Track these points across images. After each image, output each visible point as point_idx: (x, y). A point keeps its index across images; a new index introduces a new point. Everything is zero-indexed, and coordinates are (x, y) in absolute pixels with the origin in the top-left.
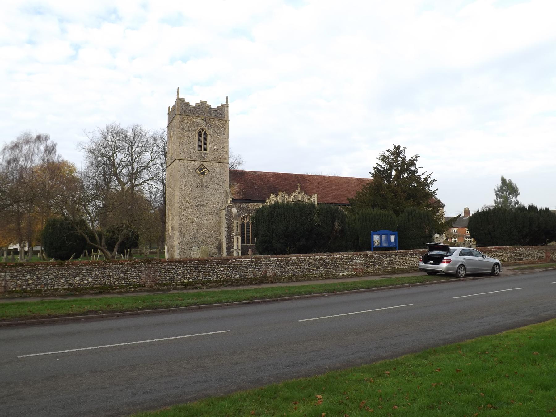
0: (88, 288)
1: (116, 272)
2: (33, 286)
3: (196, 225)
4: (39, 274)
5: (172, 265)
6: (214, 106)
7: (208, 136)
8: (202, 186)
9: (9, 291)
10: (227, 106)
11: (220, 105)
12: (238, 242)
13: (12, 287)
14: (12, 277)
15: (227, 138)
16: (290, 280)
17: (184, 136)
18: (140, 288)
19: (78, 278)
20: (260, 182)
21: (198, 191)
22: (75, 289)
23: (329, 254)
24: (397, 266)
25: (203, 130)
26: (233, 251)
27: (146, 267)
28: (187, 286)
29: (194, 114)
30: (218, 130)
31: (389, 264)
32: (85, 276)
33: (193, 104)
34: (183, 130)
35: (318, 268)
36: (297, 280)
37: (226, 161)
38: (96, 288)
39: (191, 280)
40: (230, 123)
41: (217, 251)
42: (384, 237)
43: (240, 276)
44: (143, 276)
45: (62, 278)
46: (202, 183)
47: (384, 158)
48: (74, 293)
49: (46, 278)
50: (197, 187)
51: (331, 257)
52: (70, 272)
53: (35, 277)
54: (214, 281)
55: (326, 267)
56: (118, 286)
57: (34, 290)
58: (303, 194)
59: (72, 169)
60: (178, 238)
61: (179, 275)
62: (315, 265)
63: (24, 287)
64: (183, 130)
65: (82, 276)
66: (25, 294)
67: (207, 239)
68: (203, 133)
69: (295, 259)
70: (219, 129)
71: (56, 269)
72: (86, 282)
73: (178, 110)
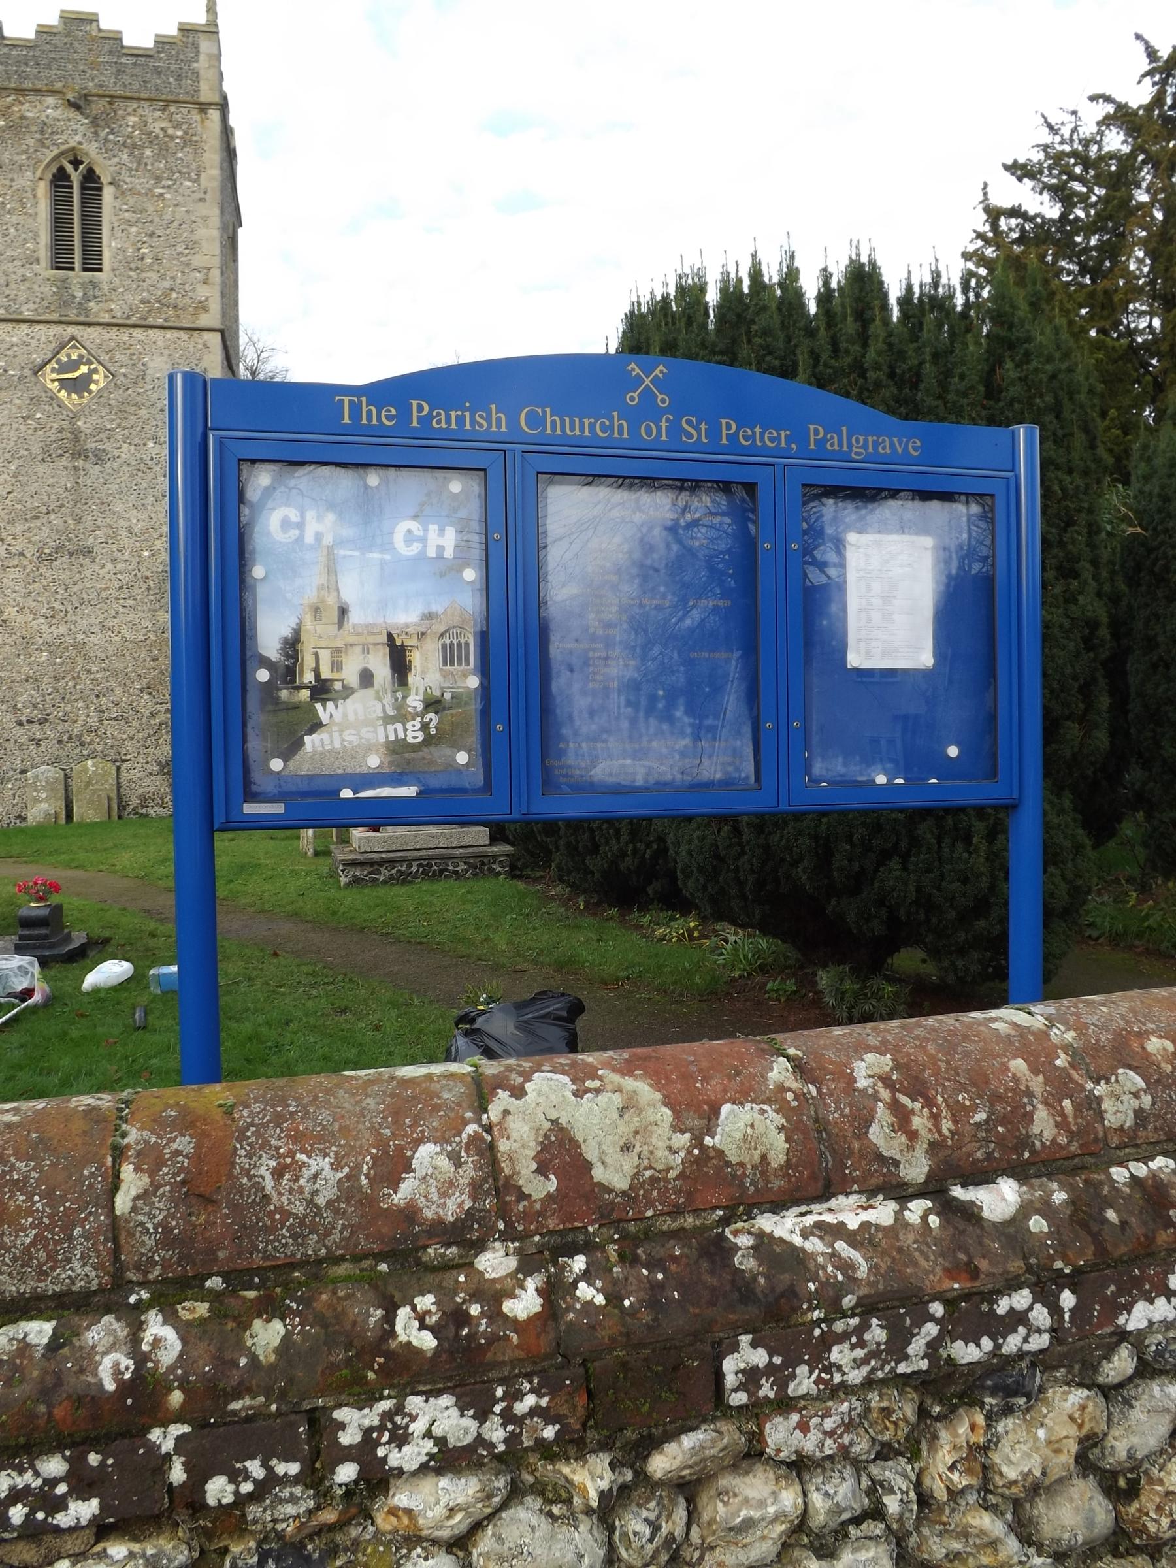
6: (139, 37)
7: (108, 193)
8: (76, 455)
10: (211, 30)
11: (53, 20)
21: (54, 478)
29: (22, 77)
30: (158, 156)
41: (165, 789)
46: (76, 435)
50: (47, 456)
67: (112, 728)
68: (76, 177)
70: (163, 151)
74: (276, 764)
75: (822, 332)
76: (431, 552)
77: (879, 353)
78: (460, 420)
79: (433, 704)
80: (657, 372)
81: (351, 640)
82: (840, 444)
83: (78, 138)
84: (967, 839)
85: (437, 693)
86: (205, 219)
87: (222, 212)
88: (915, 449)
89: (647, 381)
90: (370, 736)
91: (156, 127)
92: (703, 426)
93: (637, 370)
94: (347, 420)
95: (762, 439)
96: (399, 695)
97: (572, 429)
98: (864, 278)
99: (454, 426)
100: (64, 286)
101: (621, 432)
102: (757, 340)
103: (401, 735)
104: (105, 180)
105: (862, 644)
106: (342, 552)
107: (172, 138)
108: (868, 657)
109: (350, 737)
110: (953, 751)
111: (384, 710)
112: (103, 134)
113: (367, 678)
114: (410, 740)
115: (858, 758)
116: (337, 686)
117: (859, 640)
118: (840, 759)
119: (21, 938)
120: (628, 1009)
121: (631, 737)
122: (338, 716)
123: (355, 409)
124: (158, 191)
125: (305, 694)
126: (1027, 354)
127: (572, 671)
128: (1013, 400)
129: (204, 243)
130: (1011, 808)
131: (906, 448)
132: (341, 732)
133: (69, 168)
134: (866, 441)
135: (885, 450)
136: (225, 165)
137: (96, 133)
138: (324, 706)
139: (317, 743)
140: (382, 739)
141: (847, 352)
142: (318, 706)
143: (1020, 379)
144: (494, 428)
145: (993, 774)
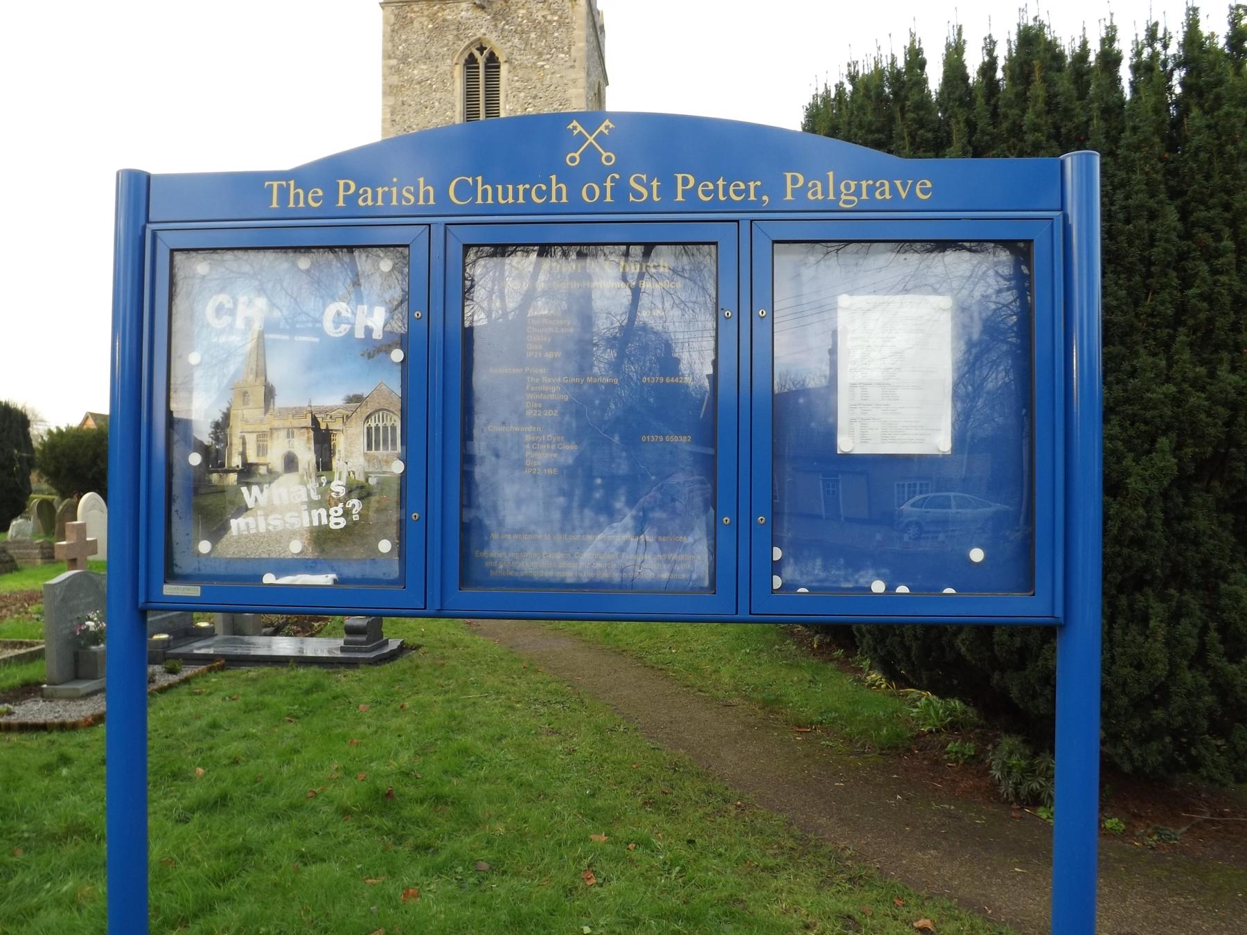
3: (470, 515)
17: (411, 81)
30: (540, 38)
34: (404, 59)
64: (404, 59)
68: (481, 60)
70: (544, 33)
74: (204, 547)
75: (980, 101)
76: (360, 334)
77: (1038, 115)
78: (387, 196)
79: (360, 490)
80: (602, 128)
81: (277, 423)
82: (825, 191)
83: (483, 31)
84: (1145, 620)
85: (362, 479)
86: (574, 81)
87: (588, 75)
88: (924, 191)
89: (591, 139)
90: (278, 523)
92: (655, 183)
93: (580, 128)
94: (275, 205)
95: (726, 193)
96: (324, 479)
97: (505, 197)
98: (1032, 41)
99: (380, 203)
101: (559, 196)
102: (911, 115)
103: (324, 521)
104: (501, 60)
105: (857, 426)
106: (272, 336)
107: (550, 22)
108: (864, 440)
109: (276, 522)
110: (977, 555)
111: (309, 496)
112: (500, 26)
113: (291, 463)
114: (333, 527)
115: (842, 561)
116: (263, 470)
117: (853, 421)
118: (819, 562)
119: (345, 643)
120: (807, 756)
121: (562, 531)
122: (263, 499)
123: (284, 192)
124: (540, 63)
125: (233, 477)
126: (1218, 98)
127: (497, 456)
128: (1198, 149)
129: (573, 100)
130: (1050, 632)
131: (912, 192)
132: (266, 516)
133: (477, 54)
134: (859, 187)
135: (884, 194)
136: (592, 39)
137: (496, 25)
138: (250, 490)
139: (243, 527)
140: (306, 524)
141: (1006, 116)
142: (244, 489)
143: (1209, 127)
144: (421, 202)
145: (1028, 584)
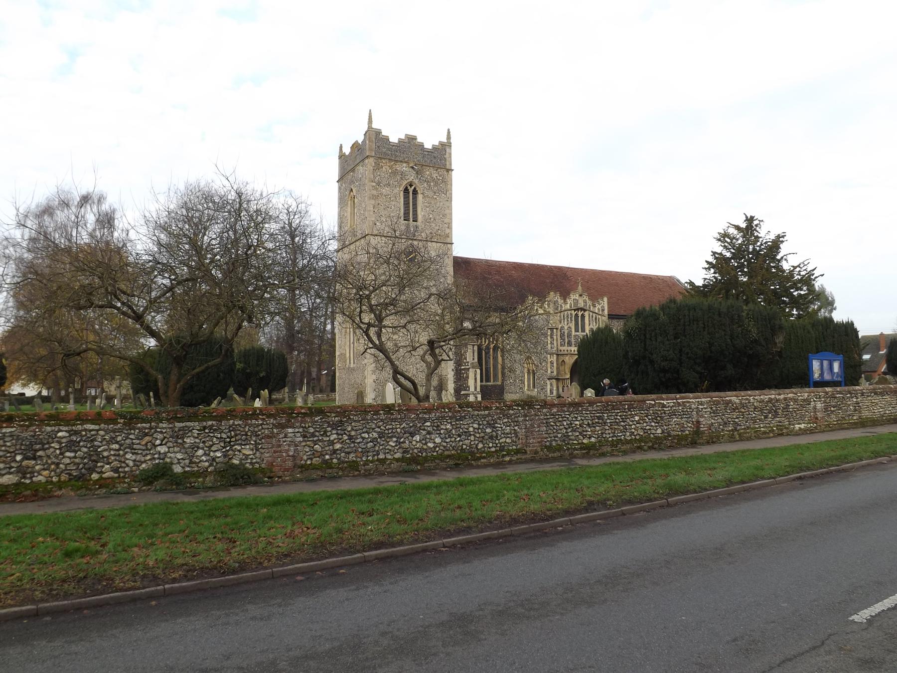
0: (435, 458)
1: (479, 425)
2: (343, 454)
4: (352, 429)
5: (564, 411)
7: (420, 197)
9: (302, 466)
12: (476, 379)
13: (305, 458)
14: (304, 436)
15: (449, 200)
16: (732, 439)
17: (381, 194)
18: (519, 456)
19: (417, 438)
20: (497, 277)
22: (414, 460)
23: (778, 391)
24: (866, 414)
25: (411, 186)
26: (468, 395)
27: (525, 416)
28: (589, 451)
31: (855, 410)
32: (429, 433)
33: (394, 139)
34: (379, 184)
35: (766, 417)
36: (742, 439)
37: (448, 241)
38: (449, 456)
39: (593, 440)
40: (455, 175)
42: (825, 363)
43: (663, 432)
44: (522, 432)
45: (391, 437)
47: (723, 237)
48: (414, 467)
49: (363, 438)
51: (782, 397)
52: (404, 425)
53: (345, 437)
54: (628, 442)
55: (776, 415)
56: (484, 452)
57: (344, 462)
58: (585, 298)
59: (294, 236)
60: (374, 372)
61: (575, 431)
62: (761, 410)
63: (327, 457)
64: (379, 184)
65: (424, 432)
66: (330, 471)
68: (411, 190)
69: (671, 403)
70: (436, 184)
71: (382, 420)
72: (431, 445)
73: (370, 150)
91: (434, 176)
100: (408, 226)
110: (866, 357)
